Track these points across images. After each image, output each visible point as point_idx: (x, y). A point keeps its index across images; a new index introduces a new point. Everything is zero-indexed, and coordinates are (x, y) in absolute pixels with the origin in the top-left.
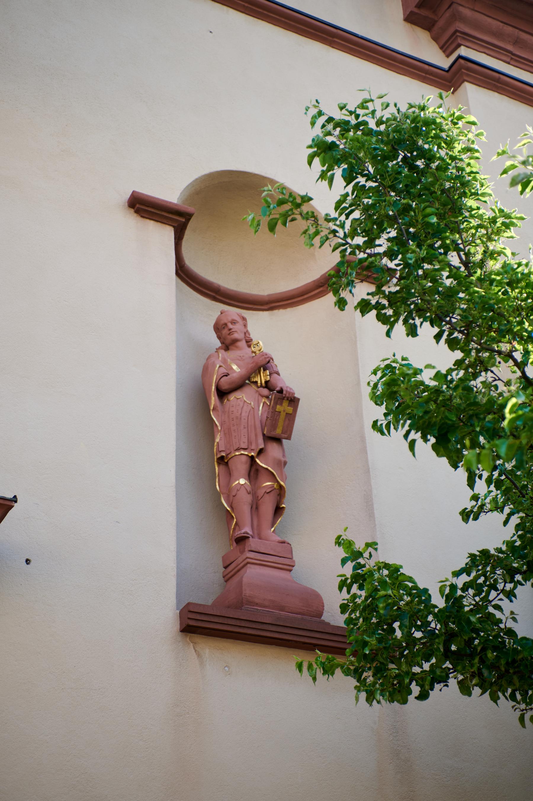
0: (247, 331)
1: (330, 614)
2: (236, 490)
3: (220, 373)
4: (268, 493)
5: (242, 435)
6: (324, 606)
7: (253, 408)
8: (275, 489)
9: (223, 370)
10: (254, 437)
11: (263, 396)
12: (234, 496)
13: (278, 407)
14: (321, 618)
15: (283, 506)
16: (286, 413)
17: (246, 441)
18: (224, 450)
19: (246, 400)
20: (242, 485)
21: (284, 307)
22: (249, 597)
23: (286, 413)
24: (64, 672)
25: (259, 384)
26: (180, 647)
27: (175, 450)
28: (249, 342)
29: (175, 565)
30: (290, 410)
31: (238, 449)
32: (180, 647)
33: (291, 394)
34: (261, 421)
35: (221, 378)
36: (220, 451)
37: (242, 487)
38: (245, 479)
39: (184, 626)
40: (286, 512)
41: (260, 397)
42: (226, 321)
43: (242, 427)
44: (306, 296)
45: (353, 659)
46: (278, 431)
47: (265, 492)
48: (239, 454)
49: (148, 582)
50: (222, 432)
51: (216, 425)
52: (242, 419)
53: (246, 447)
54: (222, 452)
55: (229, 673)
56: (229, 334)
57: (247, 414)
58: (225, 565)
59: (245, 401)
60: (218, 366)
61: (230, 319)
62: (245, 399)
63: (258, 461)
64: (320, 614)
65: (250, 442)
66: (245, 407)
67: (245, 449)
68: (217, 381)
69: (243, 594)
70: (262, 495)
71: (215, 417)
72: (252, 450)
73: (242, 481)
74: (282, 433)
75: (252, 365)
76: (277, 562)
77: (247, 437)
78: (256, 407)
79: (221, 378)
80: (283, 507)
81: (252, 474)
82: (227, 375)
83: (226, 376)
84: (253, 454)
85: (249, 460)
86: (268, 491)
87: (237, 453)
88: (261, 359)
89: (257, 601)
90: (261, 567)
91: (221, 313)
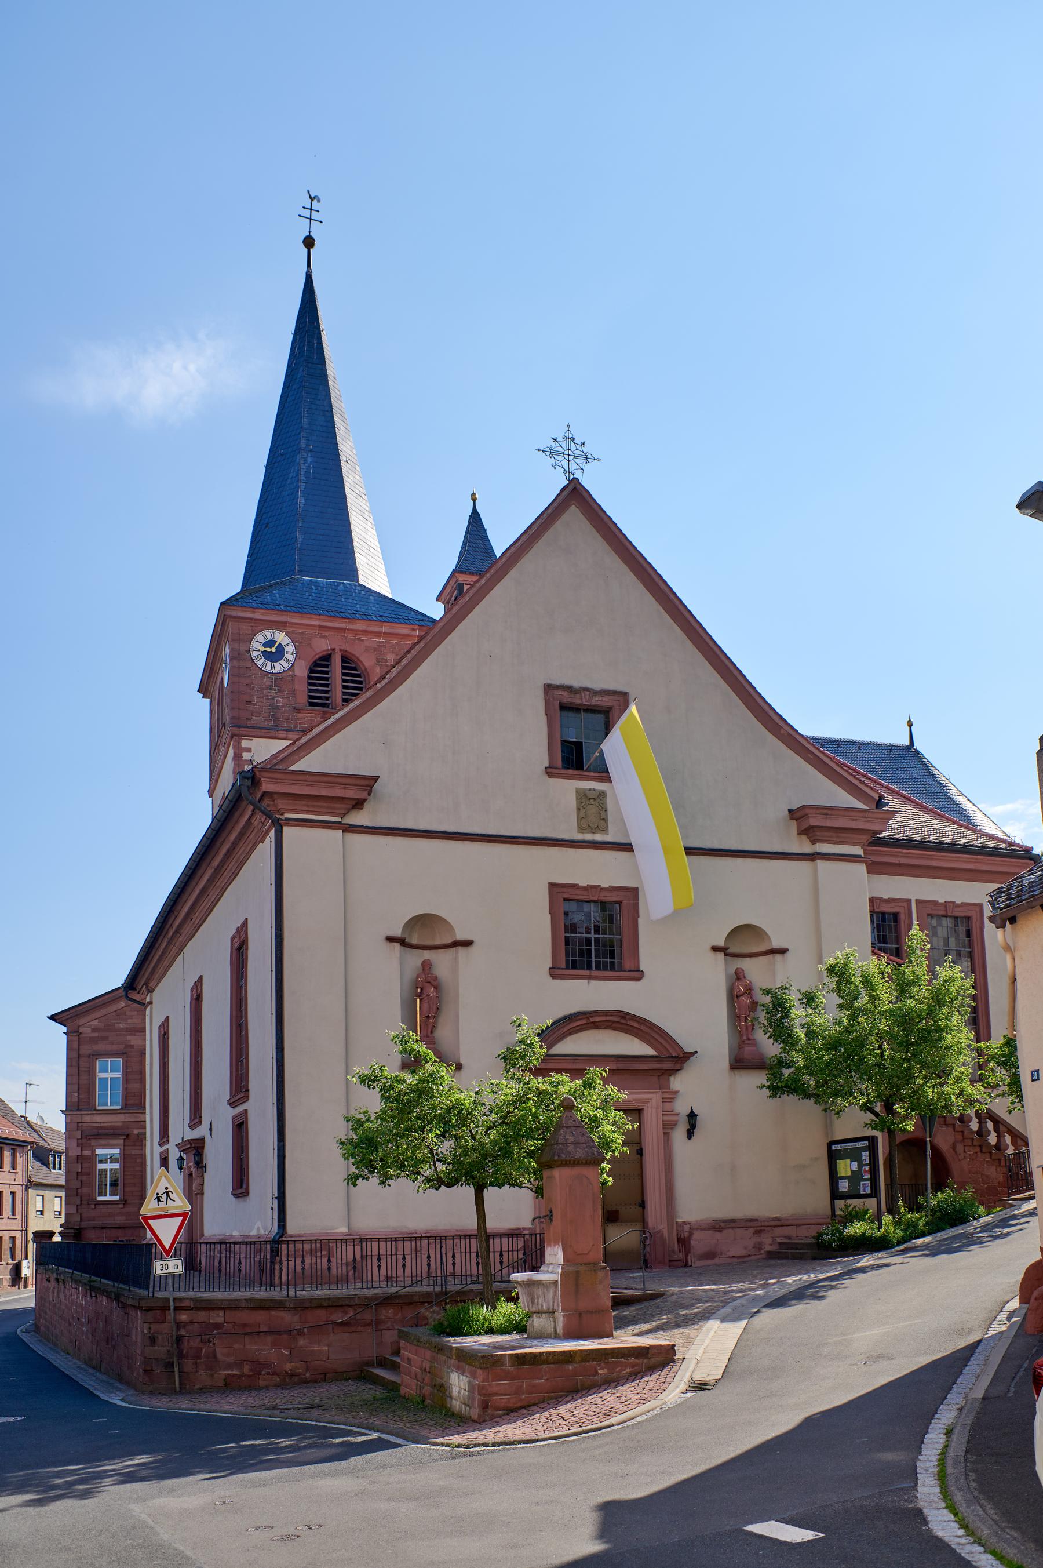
28: (745, 977)
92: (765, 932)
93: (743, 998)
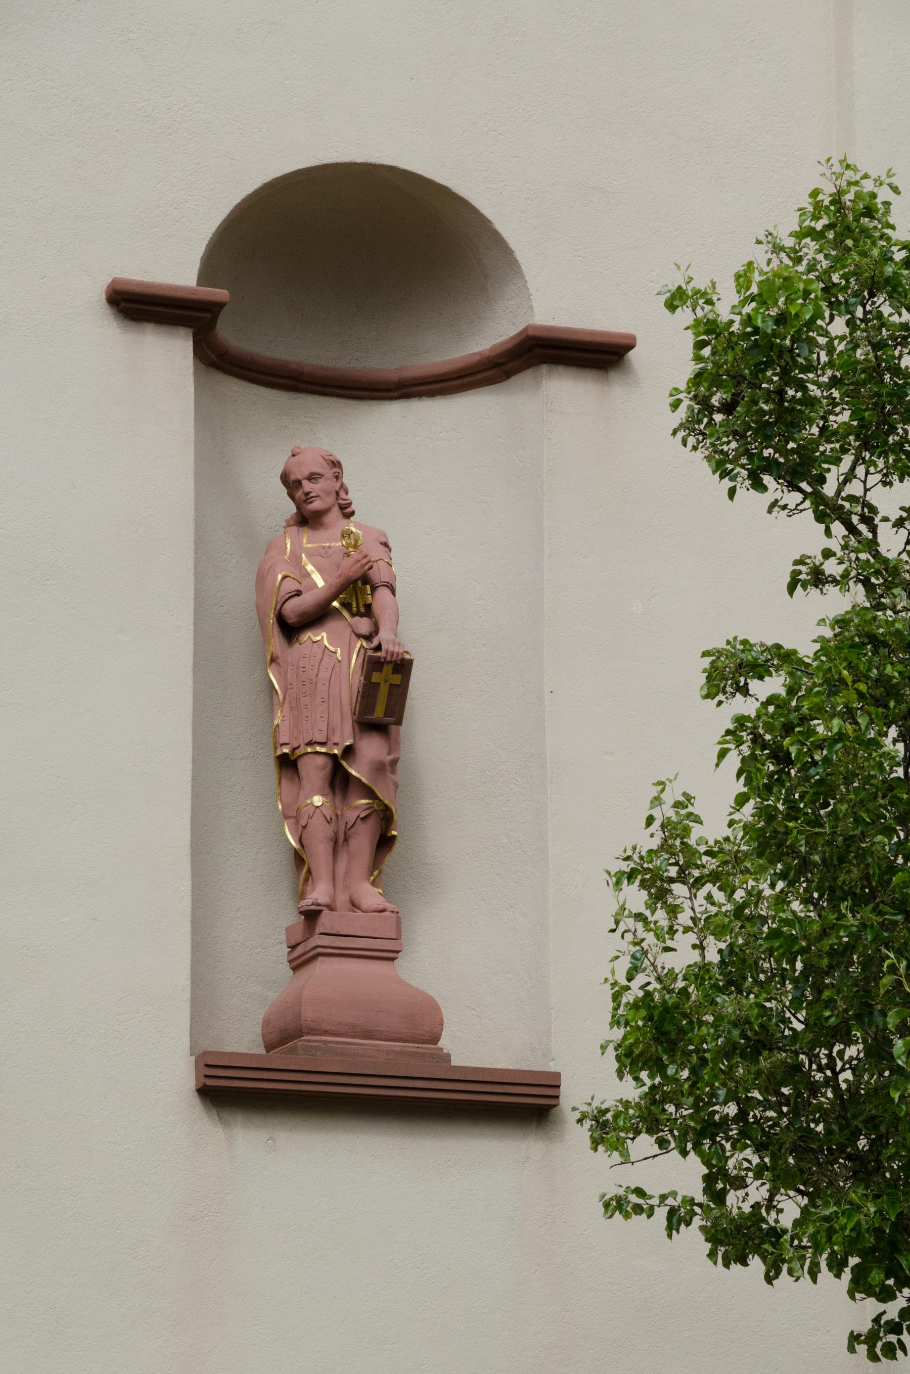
0: (342, 485)
1: (474, 1013)
2: (306, 817)
3: (282, 593)
4: (363, 819)
5: (318, 717)
6: (443, 1025)
7: (340, 661)
8: (375, 810)
9: (290, 586)
10: (339, 720)
11: (359, 636)
12: (304, 827)
13: (374, 674)
14: (436, 1044)
15: (394, 833)
16: (391, 685)
17: (324, 728)
18: (286, 742)
19: (328, 645)
20: (317, 807)
21: (431, 394)
22: (313, 1021)
23: (391, 685)
24: (19, 1167)
25: (354, 609)
26: (196, 1115)
27: (190, 779)
28: (347, 512)
29: (189, 983)
30: (397, 679)
31: (310, 744)
32: (196, 1115)
33: (395, 655)
34: (351, 688)
35: (287, 600)
36: (282, 745)
37: (318, 809)
38: (322, 795)
39: (201, 1085)
40: (397, 846)
41: (353, 636)
42: (299, 477)
43: (319, 700)
44: (466, 380)
45: (761, 861)
46: (379, 713)
47: (359, 816)
48: (313, 751)
49: (145, 1014)
50: (286, 705)
51: (276, 691)
52: (319, 684)
53: (325, 740)
54: (284, 746)
55: (274, 1149)
56: (305, 501)
57: (329, 674)
58: (293, 943)
59: (326, 647)
60: (280, 577)
61: (306, 472)
62: (326, 643)
63: (344, 764)
64: (435, 1039)
65: (330, 729)
66: (326, 660)
67: (322, 744)
68: (278, 608)
69: (303, 1018)
70: (353, 821)
71: (274, 676)
72: (335, 744)
73: (318, 800)
74: (385, 716)
75: (338, 580)
76: (369, 947)
77: (325, 719)
78: (345, 663)
79: (287, 600)
80: (394, 837)
81: (337, 782)
82: (298, 593)
83: (298, 595)
84: (336, 751)
85: (329, 764)
86: (362, 815)
87: (309, 750)
88: (354, 569)
89: (325, 1027)
90: (343, 959)
91: (293, 455)
92: (483, 223)
93: (321, 636)
